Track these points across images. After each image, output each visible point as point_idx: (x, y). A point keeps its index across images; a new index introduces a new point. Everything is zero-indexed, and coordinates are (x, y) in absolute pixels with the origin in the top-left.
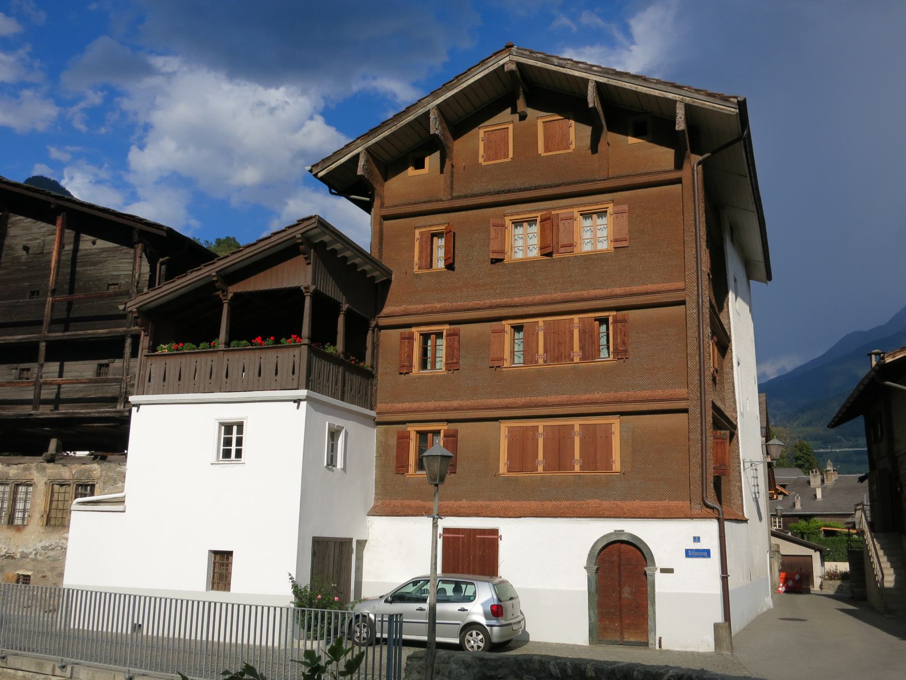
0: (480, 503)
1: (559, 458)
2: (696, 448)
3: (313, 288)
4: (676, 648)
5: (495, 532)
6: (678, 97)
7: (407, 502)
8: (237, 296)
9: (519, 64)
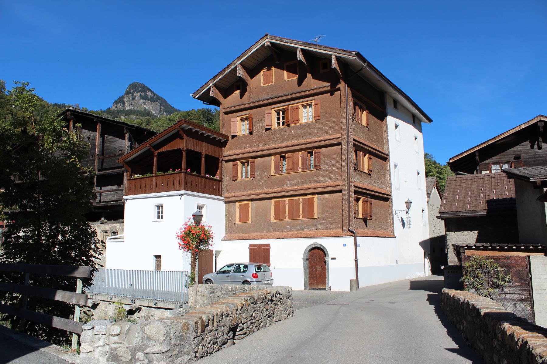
0: (264, 234)
1: (293, 214)
2: (345, 206)
3: (185, 149)
5: (268, 245)
6: (332, 53)
7: (237, 235)
8: (159, 154)
9: (271, 42)
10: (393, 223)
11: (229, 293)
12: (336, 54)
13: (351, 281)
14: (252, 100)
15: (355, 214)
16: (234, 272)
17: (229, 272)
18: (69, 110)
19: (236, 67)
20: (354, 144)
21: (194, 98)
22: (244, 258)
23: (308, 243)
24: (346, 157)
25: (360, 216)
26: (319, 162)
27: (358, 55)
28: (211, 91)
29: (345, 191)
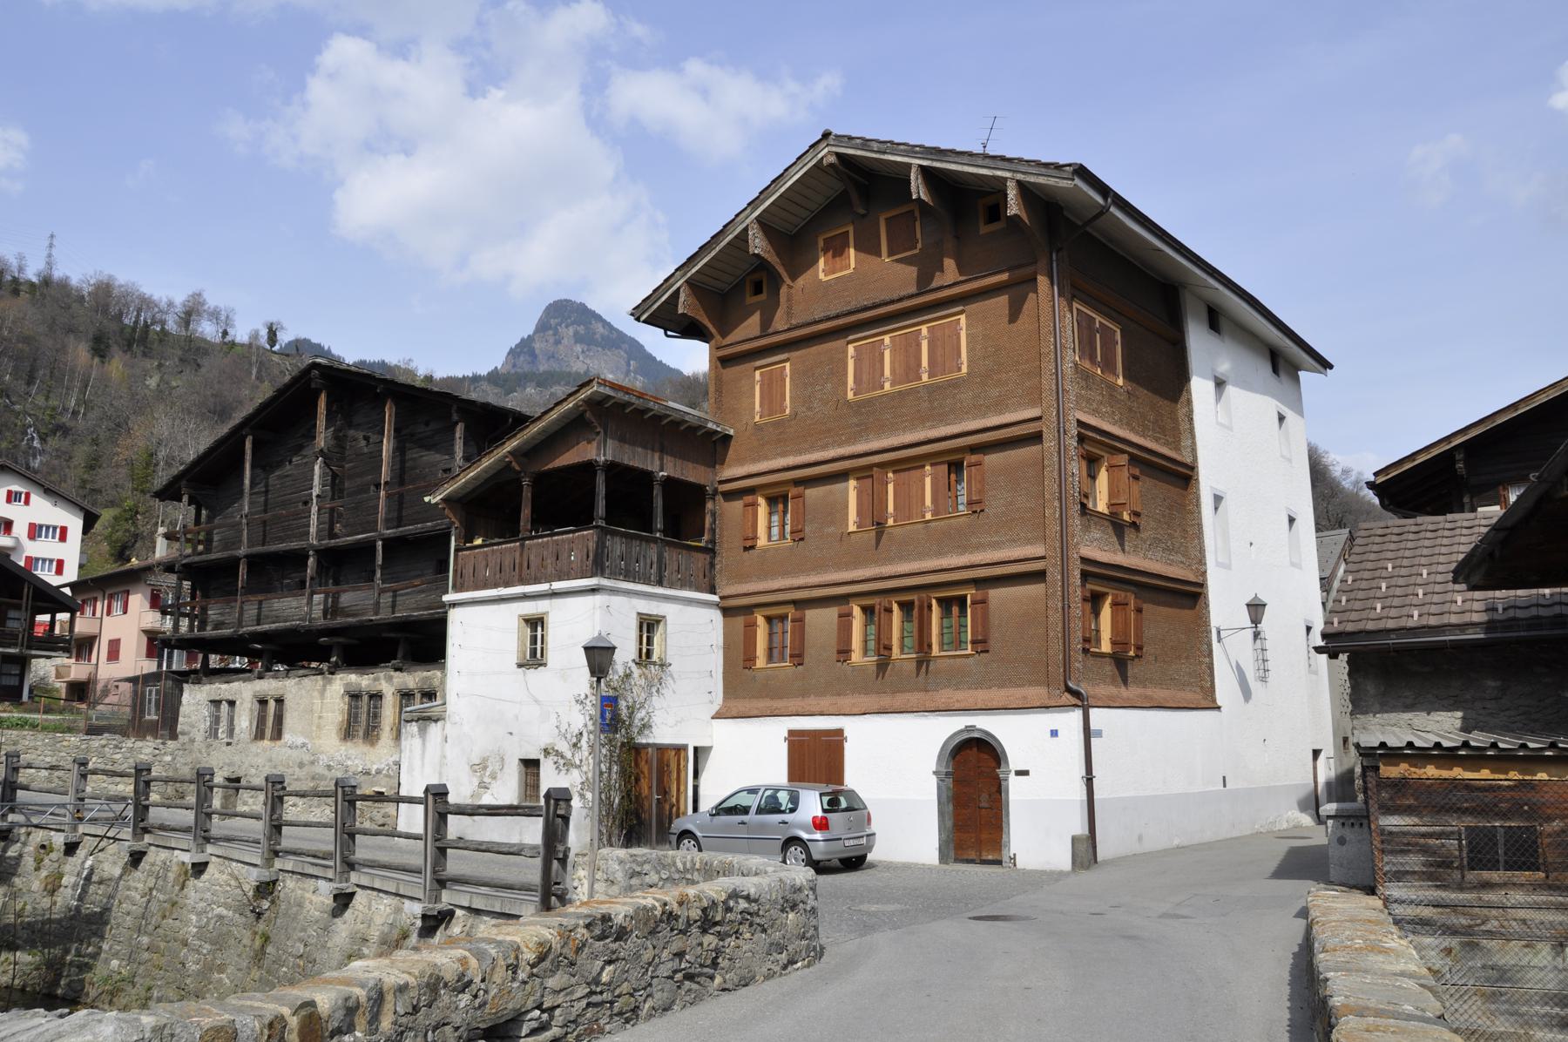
4: (1029, 867)
5: (840, 732)
6: (1008, 175)
9: (838, 155)
10: (1211, 667)
11: (676, 876)
12: (1020, 177)
13: (1075, 840)
14: (794, 322)
15: (1086, 640)
16: (760, 811)
17: (746, 810)
18: (315, 366)
19: (746, 229)
20: (1079, 434)
21: (638, 319)
22: (773, 769)
23: (949, 726)
24: (1056, 474)
25: (1106, 647)
26: (981, 492)
27: (1082, 172)
28: (682, 299)
29: (1054, 575)
